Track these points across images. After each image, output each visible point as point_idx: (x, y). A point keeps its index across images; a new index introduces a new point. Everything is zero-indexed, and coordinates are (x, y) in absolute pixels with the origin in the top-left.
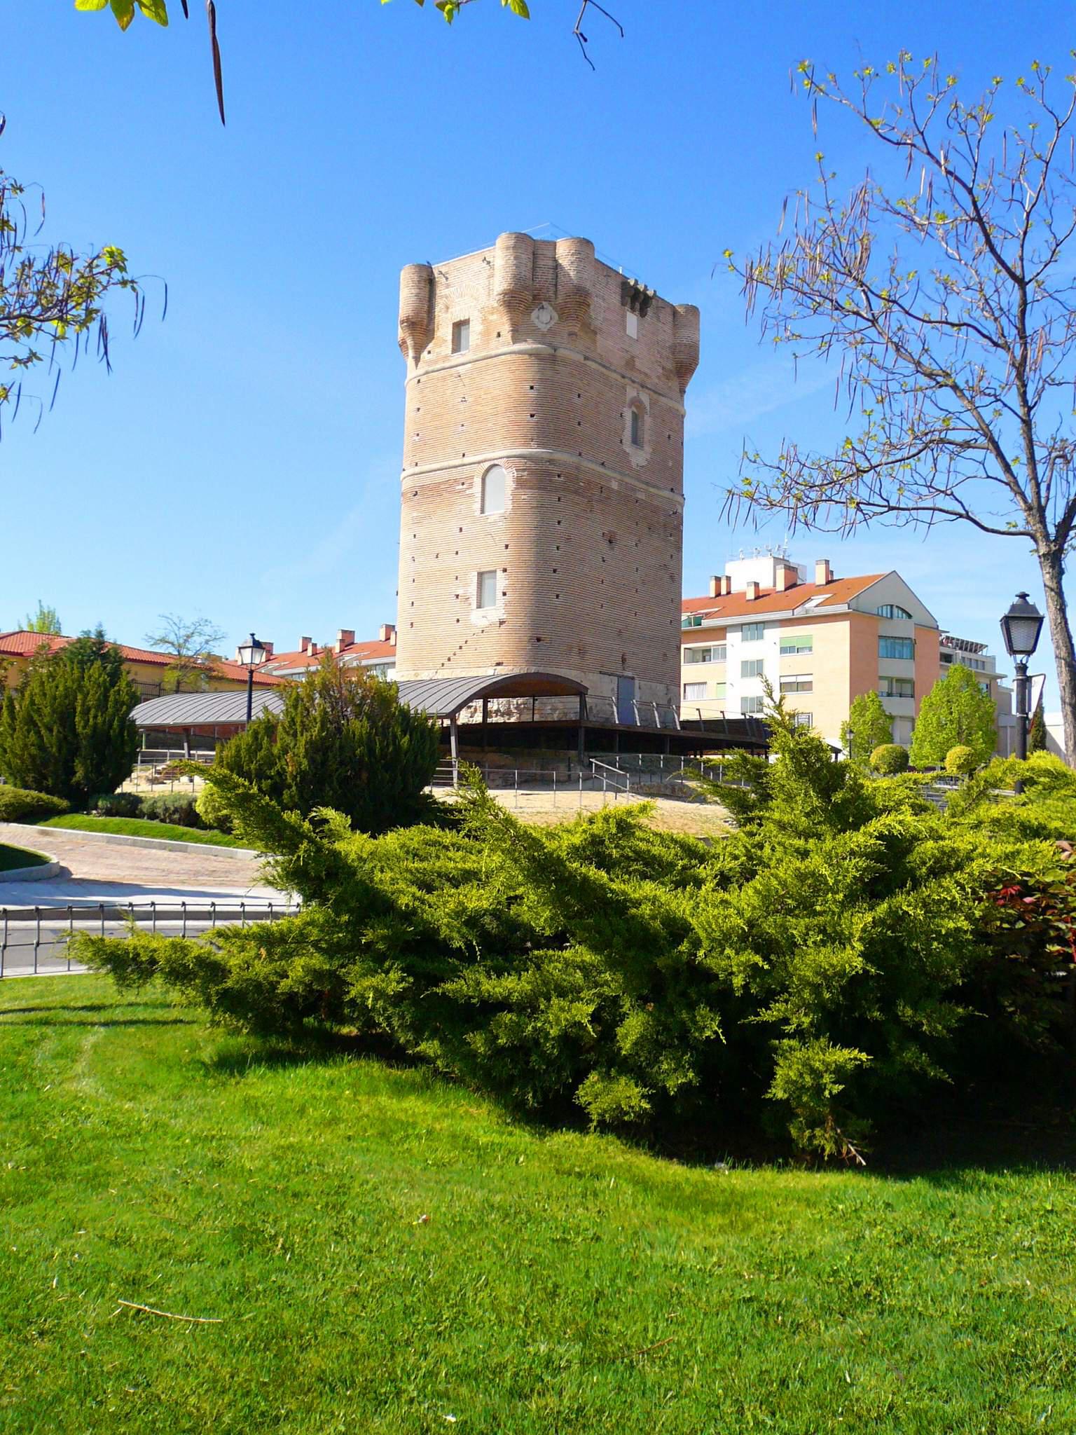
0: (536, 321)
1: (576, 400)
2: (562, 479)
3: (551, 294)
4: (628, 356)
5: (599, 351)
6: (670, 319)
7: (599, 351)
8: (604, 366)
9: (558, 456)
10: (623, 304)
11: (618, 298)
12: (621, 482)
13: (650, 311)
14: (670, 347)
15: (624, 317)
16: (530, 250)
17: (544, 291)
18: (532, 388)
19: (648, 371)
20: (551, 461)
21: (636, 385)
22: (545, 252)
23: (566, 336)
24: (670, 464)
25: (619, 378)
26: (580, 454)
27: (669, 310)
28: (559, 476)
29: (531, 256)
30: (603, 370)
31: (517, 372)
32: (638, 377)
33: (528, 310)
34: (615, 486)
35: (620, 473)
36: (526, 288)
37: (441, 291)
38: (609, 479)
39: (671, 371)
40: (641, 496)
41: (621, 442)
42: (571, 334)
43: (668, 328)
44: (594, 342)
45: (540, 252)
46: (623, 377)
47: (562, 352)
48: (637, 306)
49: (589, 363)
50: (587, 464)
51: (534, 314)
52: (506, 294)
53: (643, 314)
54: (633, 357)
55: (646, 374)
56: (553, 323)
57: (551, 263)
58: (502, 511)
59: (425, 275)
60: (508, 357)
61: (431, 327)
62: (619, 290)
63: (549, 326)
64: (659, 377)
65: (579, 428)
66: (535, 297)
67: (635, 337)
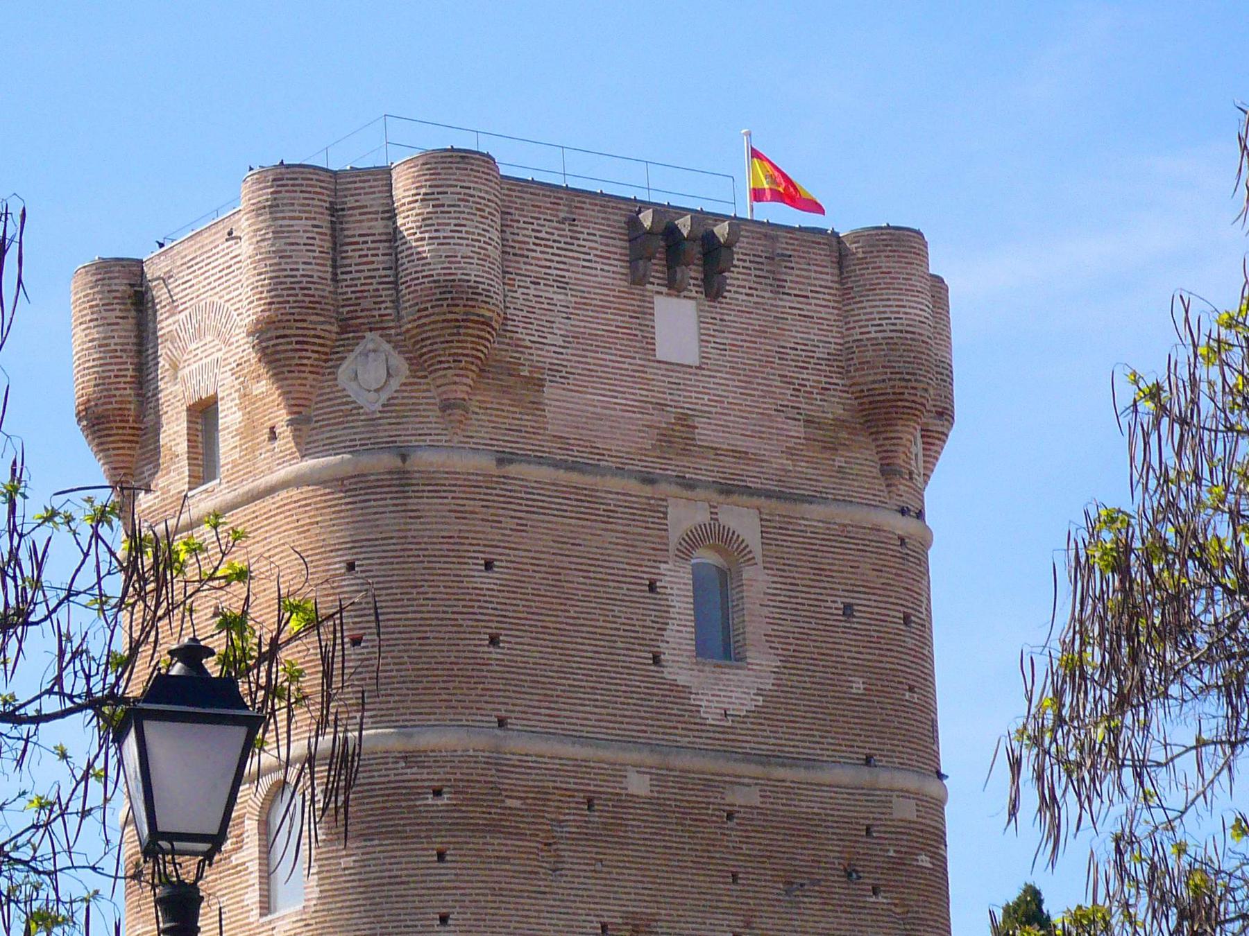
0: (352, 389)
1: (483, 580)
2: (445, 800)
3: (387, 308)
4: (662, 420)
5: (552, 429)
6: (828, 277)
7: (552, 429)
8: (572, 467)
9: (427, 740)
10: (637, 279)
11: (620, 267)
12: (659, 779)
13: (736, 279)
14: (831, 358)
15: (645, 313)
16: (320, 204)
17: (366, 304)
18: (351, 566)
19: (742, 444)
20: (408, 758)
21: (700, 493)
22: (365, 200)
23: (434, 414)
24: (858, 686)
25: (633, 486)
26: (502, 723)
27: (822, 255)
28: (438, 793)
29: (325, 221)
30: (575, 478)
31: (316, 530)
32: (705, 470)
33: (331, 357)
34: (638, 785)
35: (653, 747)
36: (314, 305)
37: (166, 324)
38: (618, 771)
39: (840, 423)
40: (740, 797)
41: (656, 660)
42: (447, 406)
43: (823, 306)
44: (537, 406)
45: (351, 202)
46: (649, 480)
47: (425, 460)
48: (693, 273)
49: (512, 470)
50: (517, 744)
51: (344, 372)
52: (261, 332)
53: (713, 289)
54: (683, 419)
55: (742, 455)
56: (395, 384)
57: (379, 227)
58: (299, 907)
59: (121, 286)
60: (294, 493)
61: (150, 419)
62: (619, 246)
63: (384, 397)
64: (790, 453)
65: (495, 653)
66: (345, 326)
67: (692, 358)
